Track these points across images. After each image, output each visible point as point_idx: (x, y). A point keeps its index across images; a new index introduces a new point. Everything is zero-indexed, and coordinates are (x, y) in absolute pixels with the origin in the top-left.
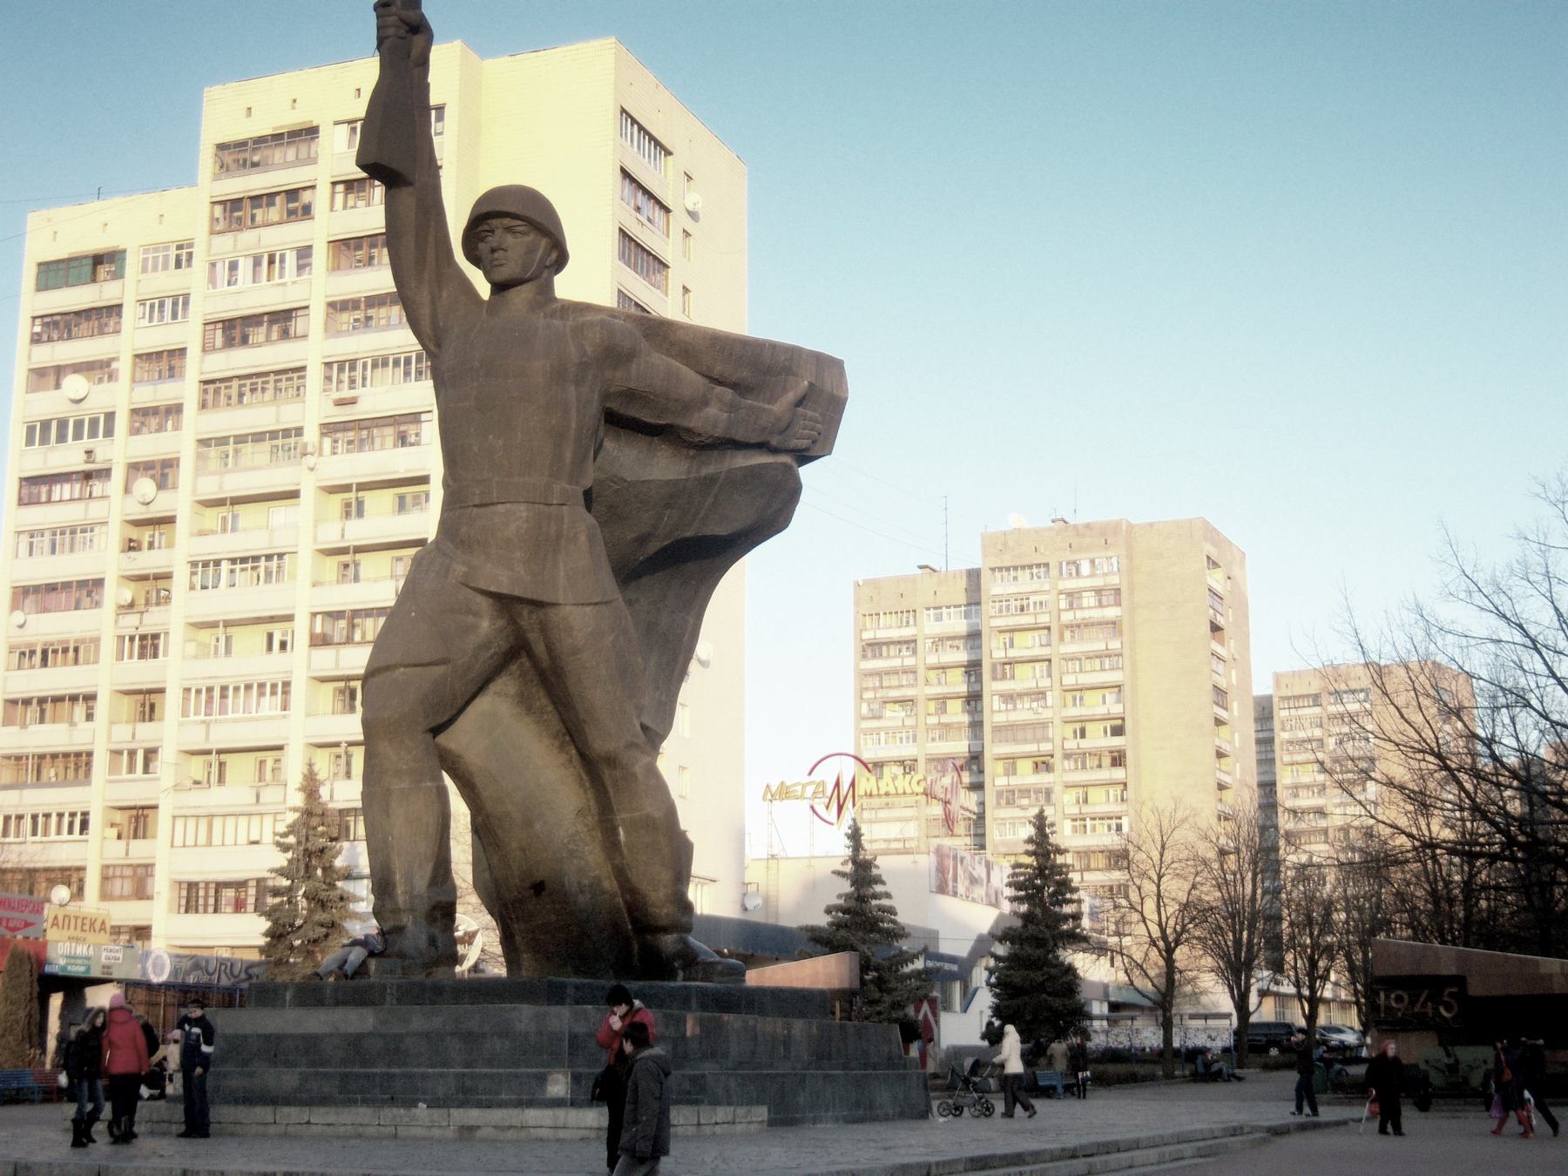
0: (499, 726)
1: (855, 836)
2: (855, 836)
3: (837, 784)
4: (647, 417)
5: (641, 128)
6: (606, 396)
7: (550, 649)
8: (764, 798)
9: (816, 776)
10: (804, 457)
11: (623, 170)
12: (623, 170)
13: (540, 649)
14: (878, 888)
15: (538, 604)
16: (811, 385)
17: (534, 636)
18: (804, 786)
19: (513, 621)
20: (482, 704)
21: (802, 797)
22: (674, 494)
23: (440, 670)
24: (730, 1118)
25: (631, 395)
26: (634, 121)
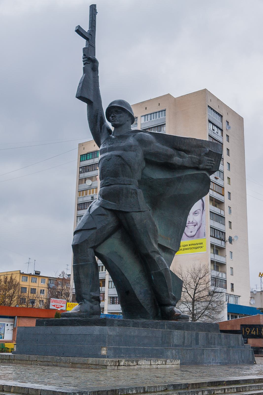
0: (114, 246)
8: (259, 276)
20: (110, 241)
23: (93, 232)
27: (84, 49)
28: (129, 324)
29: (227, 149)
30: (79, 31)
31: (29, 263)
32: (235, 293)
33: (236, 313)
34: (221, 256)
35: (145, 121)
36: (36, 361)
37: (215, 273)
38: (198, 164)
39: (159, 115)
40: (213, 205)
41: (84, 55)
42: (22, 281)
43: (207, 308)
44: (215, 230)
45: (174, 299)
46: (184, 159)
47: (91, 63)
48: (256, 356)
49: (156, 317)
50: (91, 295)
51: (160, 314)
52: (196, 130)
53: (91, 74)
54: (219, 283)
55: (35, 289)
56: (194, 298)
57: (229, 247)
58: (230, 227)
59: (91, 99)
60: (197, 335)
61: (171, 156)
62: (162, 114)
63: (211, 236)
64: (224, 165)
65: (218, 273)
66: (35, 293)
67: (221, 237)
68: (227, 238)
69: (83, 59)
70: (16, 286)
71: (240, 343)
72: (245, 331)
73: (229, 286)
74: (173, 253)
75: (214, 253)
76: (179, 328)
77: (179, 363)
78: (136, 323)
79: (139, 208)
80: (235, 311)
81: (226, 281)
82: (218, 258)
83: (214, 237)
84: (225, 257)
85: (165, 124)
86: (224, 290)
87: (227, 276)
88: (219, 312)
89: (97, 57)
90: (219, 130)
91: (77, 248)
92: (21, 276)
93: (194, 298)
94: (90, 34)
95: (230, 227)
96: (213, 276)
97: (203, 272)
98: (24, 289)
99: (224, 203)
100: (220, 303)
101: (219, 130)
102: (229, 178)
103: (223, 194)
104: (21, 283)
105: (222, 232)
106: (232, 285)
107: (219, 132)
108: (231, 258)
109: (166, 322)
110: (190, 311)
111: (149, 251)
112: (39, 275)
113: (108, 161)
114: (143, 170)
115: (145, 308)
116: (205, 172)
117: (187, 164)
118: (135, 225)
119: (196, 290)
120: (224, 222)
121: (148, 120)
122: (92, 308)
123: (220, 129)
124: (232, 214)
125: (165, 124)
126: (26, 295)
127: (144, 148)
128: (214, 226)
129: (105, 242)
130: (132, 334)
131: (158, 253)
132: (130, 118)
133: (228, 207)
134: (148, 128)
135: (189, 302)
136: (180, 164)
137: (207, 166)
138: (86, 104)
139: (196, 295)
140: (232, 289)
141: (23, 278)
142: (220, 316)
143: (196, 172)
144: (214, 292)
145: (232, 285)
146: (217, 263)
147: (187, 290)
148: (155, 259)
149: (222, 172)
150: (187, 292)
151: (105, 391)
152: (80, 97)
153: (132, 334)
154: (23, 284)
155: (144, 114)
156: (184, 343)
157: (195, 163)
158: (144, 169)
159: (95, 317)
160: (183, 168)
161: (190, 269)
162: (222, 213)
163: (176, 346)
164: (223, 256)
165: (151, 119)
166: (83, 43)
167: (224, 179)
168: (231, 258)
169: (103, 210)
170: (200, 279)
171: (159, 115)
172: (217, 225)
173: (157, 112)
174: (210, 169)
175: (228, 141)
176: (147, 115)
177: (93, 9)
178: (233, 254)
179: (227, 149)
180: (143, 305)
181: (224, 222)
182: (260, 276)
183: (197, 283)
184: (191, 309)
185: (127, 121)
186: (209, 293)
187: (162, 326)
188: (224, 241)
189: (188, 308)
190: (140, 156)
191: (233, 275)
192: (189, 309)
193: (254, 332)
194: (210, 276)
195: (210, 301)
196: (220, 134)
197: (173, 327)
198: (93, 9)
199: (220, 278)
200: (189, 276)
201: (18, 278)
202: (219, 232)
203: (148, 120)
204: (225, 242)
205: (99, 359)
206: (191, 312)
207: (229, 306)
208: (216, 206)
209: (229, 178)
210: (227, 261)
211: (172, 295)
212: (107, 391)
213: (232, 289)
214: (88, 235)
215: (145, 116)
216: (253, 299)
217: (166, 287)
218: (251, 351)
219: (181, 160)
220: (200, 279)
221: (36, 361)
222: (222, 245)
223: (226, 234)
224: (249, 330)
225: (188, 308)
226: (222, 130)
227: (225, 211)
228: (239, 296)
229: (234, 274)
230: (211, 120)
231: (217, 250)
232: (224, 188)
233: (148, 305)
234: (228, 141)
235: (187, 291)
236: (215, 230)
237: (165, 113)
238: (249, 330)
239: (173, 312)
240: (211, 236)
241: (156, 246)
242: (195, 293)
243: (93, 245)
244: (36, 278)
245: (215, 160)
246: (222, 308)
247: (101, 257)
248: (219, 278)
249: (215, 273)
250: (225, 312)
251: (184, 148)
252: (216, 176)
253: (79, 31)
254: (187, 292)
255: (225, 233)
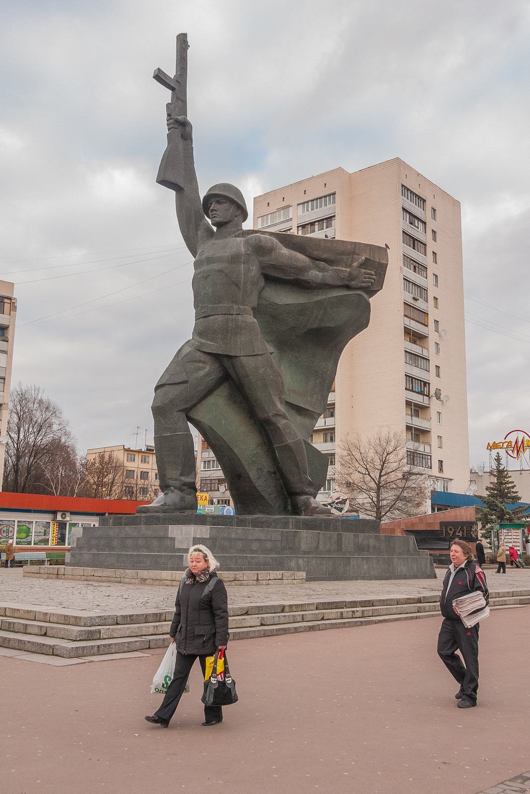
0: (219, 410)
1: (498, 460)
2: (498, 460)
3: (516, 442)
4: (280, 275)
5: (411, 192)
6: (263, 268)
7: (236, 373)
8: (487, 449)
9: (508, 439)
10: (372, 292)
11: (404, 209)
12: (404, 209)
13: (234, 376)
14: (510, 480)
15: (230, 357)
16: (366, 259)
17: (231, 371)
18: (503, 443)
19: (222, 365)
20: (211, 399)
21: (502, 448)
22: (302, 310)
23: (184, 385)
24: (280, 577)
25: (274, 267)
26: (408, 190)
27: (168, 105)
28: (231, 522)
29: (433, 252)
30: (160, 77)
31: (137, 434)
32: (445, 475)
33: (446, 506)
34: (423, 418)
35: (303, 212)
36: (94, 575)
37: (412, 445)
38: (348, 280)
39: (325, 201)
40: (410, 341)
41: (169, 115)
42: (127, 460)
43: (399, 498)
44: (414, 380)
45: (310, 484)
46: (325, 273)
47: (180, 127)
48: (438, 568)
49: (285, 510)
50: (181, 480)
51: (289, 507)
52: (371, 225)
53: (181, 145)
54: (417, 460)
55: (148, 472)
56: (379, 483)
57: (435, 405)
58: (438, 375)
59: (181, 183)
60: (340, 537)
61: (303, 270)
62: (330, 200)
63: (406, 389)
64: (428, 277)
65: (417, 444)
66: (147, 478)
67: (423, 390)
68: (432, 392)
69: (167, 121)
70: (118, 467)
71: (411, 549)
72: (446, 531)
73: (435, 465)
74: (316, 416)
75: (412, 416)
76: (308, 526)
77: (305, 578)
78: (242, 521)
79: (254, 351)
80: (443, 501)
81: (431, 456)
82: (418, 422)
83: (412, 391)
84: (429, 421)
85: (334, 216)
86: (428, 471)
87: (432, 449)
88: (419, 505)
89: (190, 118)
90: (419, 222)
91: (159, 411)
92: (126, 453)
93: (379, 482)
94: (177, 81)
95: (438, 375)
96: (409, 450)
97: (393, 444)
98: (130, 473)
99: (428, 337)
100: (421, 491)
101: (419, 222)
102: (436, 299)
103: (426, 324)
104: (127, 464)
105: (425, 383)
106: (441, 462)
107: (419, 226)
108: (439, 423)
109: (292, 518)
110: (374, 502)
111: (270, 415)
112: (152, 452)
113: (206, 279)
114: (261, 292)
115: (267, 498)
116: (359, 292)
117: (330, 281)
118: (247, 376)
119: (383, 471)
120: (428, 368)
121: (308, 210)
122: (182, 499)
123: (421, 221)
124: (440, 354)
125: (334, 216)
126: (133, 481)
127: (261, 259)
128: (412, 374)
129: (204, 402)
130: (233, 536)
131: (284, 417)
132: (240, 212)
133: (434, 343)
134: (308, 222)
135: (372, 490)
136: (319, 281)
137: (363, 283)
138: (173, 193)
139: (382, 479)
140: (441, 470)
141: (128, 457)
142: (422, 509)
143: (346, 293)
144: (410, 473)
145: (441, 462)
146: (416, 429)
147: (368, 472)
148: (279, 425)
149: (424, 289)
150: (369, 474)
151: (143, 615)
152: (163, 181)
153: (233, 536)
154: (130, 465)
155: (303, 201)
156: (318, 547)
157: (343, 278)
158: (262, 290)
159: (188, 513)
160: (324, 286)
161: (372, 440)
162: (425, 353)
163: (305, 553)
164: (426, 419)
165: (312, 209)
166: (166, 95)
167: (429, 301)
168: (439, 423)
169: (199, 353)
170: (388, 454)
171: (325, 201)
172: (416, 372)
173: (322, 198)
174: (368, 287)
175: (435, 239)
176: (307, 202)
177: (182, 42)
178: (442, 415)
179: (433, 252)
180: (263, 494)
181: (428, 368)
182: (489, 448)
183: (384, 460)
184: (375, 499)
185: (236, 216)
186: (404, 476)
187: (285, 525)
188: (428, 396)
189: (370, 498)
190: (255, 270)
191: (441, 448)
192: (372, 499)
193: (461, 532)
194: (405, 450)
195: (404, 489)
196: (422, 229)
197: (303, 525)
198: (182, 42)
199: (420, 452)
200: (371, 451)
201: (120, 456)
202: (419, 382)
203: (308, 210)
204: (429, 398)
205: (176, 572)
206: (374, 503)
207: (434, 492)
208: (415, 342)
209: (436, 299)
210: (432, 427)
211: (307, 478)
212: (146, 616)
213: (441, 470)
214: (173, 392)
215: (303, 203)
216: (473, 484)
217: (298, 467)
218: (429, 560)
219: (320, 274)
220: (388, 454)
221: (94, 575)
222: (424, 402)
223: (431, 386)
224: (453, 530)
225: (370, 498)
226: (424, 223)
227: (430, 350)
228: (451, 480)
229: (443, 446)
230: (407, 207)
231: (417, 409)
232: (428, 314)
233: (270, 494)
234: (435, 239)
235: (369, 473)
236: (414, 380)
237: (334, 199)
238: (453, 530)
239: (307, 505)
240: (406, 389)
241: (281, 408)
242: (380, 476)
243: (182, 407)
244: (134, 455)
245: (375, 272)
246: (424, 498)
247: (197, 424)
248: (418, 452)
249: (412, 445)
250: (429, 503)
251: (325, 256)
252: (414, 296)
253: (160, 77)
254: (369, 474)
255: (429, 384)
